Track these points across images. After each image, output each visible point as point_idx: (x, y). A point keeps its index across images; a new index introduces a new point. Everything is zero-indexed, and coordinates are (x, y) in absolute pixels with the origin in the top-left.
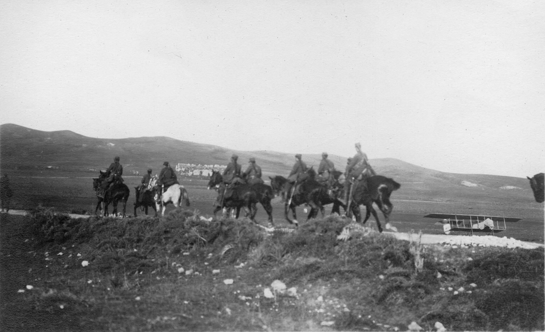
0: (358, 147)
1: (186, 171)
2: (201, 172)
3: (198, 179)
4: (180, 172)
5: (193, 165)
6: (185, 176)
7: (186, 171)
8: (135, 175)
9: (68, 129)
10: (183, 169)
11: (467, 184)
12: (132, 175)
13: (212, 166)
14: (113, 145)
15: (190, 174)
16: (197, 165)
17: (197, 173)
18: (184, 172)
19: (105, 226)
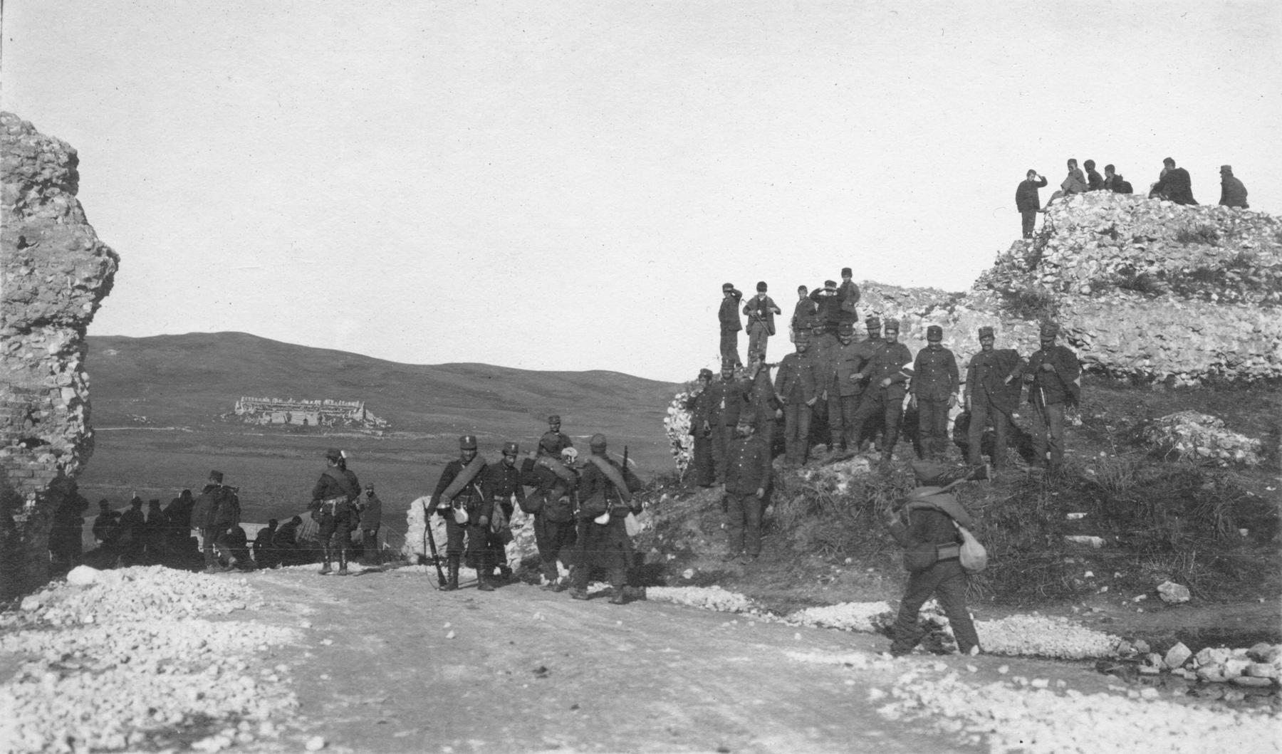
0: (847, 272)
1: (258, 414)
2: (289, 418)
3: (281, 431)
4: (244, 415)
5: (276, 400)
6: (252, 425)
7: (258, 414)
8: (138, 424)
9: (162, 333)
10: (252, 411)
11: (1194, 432)
12: (132, 423)
13: (318, 402)
14: (113, 352)
15: (265, 420)
16: (286, 399)
17: (279, 418)
18: (252, 416)
19: (394, 456)
